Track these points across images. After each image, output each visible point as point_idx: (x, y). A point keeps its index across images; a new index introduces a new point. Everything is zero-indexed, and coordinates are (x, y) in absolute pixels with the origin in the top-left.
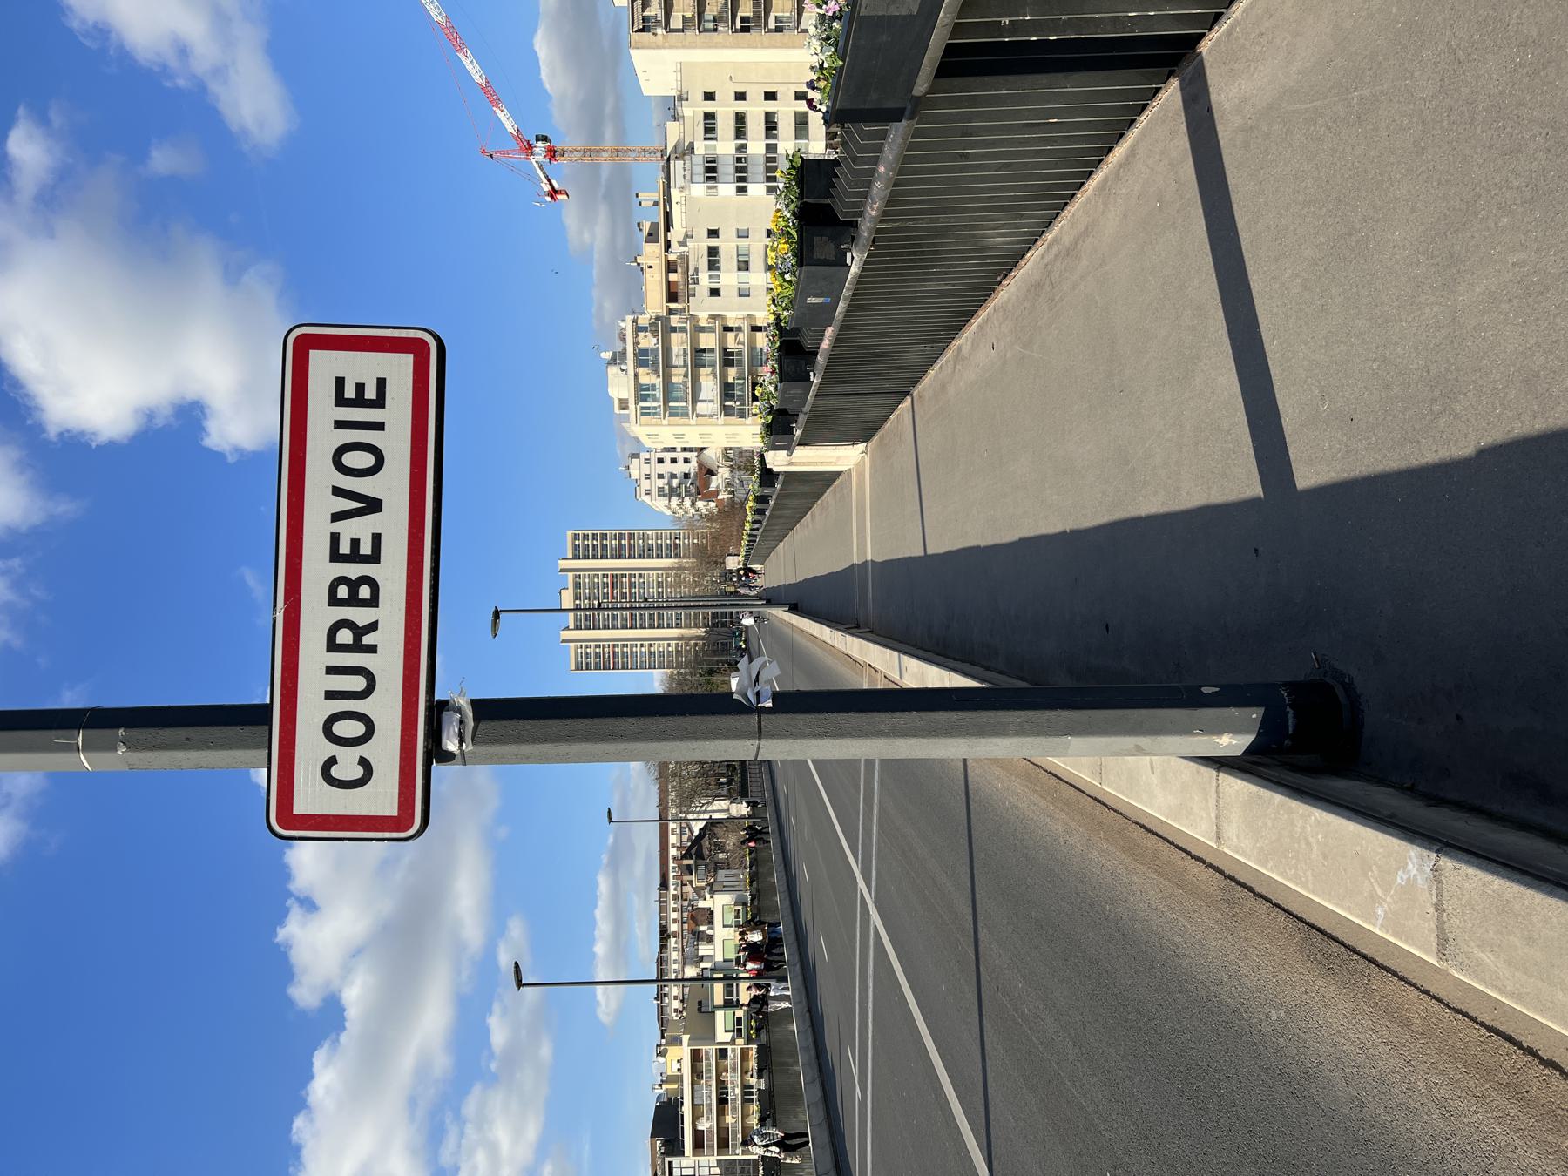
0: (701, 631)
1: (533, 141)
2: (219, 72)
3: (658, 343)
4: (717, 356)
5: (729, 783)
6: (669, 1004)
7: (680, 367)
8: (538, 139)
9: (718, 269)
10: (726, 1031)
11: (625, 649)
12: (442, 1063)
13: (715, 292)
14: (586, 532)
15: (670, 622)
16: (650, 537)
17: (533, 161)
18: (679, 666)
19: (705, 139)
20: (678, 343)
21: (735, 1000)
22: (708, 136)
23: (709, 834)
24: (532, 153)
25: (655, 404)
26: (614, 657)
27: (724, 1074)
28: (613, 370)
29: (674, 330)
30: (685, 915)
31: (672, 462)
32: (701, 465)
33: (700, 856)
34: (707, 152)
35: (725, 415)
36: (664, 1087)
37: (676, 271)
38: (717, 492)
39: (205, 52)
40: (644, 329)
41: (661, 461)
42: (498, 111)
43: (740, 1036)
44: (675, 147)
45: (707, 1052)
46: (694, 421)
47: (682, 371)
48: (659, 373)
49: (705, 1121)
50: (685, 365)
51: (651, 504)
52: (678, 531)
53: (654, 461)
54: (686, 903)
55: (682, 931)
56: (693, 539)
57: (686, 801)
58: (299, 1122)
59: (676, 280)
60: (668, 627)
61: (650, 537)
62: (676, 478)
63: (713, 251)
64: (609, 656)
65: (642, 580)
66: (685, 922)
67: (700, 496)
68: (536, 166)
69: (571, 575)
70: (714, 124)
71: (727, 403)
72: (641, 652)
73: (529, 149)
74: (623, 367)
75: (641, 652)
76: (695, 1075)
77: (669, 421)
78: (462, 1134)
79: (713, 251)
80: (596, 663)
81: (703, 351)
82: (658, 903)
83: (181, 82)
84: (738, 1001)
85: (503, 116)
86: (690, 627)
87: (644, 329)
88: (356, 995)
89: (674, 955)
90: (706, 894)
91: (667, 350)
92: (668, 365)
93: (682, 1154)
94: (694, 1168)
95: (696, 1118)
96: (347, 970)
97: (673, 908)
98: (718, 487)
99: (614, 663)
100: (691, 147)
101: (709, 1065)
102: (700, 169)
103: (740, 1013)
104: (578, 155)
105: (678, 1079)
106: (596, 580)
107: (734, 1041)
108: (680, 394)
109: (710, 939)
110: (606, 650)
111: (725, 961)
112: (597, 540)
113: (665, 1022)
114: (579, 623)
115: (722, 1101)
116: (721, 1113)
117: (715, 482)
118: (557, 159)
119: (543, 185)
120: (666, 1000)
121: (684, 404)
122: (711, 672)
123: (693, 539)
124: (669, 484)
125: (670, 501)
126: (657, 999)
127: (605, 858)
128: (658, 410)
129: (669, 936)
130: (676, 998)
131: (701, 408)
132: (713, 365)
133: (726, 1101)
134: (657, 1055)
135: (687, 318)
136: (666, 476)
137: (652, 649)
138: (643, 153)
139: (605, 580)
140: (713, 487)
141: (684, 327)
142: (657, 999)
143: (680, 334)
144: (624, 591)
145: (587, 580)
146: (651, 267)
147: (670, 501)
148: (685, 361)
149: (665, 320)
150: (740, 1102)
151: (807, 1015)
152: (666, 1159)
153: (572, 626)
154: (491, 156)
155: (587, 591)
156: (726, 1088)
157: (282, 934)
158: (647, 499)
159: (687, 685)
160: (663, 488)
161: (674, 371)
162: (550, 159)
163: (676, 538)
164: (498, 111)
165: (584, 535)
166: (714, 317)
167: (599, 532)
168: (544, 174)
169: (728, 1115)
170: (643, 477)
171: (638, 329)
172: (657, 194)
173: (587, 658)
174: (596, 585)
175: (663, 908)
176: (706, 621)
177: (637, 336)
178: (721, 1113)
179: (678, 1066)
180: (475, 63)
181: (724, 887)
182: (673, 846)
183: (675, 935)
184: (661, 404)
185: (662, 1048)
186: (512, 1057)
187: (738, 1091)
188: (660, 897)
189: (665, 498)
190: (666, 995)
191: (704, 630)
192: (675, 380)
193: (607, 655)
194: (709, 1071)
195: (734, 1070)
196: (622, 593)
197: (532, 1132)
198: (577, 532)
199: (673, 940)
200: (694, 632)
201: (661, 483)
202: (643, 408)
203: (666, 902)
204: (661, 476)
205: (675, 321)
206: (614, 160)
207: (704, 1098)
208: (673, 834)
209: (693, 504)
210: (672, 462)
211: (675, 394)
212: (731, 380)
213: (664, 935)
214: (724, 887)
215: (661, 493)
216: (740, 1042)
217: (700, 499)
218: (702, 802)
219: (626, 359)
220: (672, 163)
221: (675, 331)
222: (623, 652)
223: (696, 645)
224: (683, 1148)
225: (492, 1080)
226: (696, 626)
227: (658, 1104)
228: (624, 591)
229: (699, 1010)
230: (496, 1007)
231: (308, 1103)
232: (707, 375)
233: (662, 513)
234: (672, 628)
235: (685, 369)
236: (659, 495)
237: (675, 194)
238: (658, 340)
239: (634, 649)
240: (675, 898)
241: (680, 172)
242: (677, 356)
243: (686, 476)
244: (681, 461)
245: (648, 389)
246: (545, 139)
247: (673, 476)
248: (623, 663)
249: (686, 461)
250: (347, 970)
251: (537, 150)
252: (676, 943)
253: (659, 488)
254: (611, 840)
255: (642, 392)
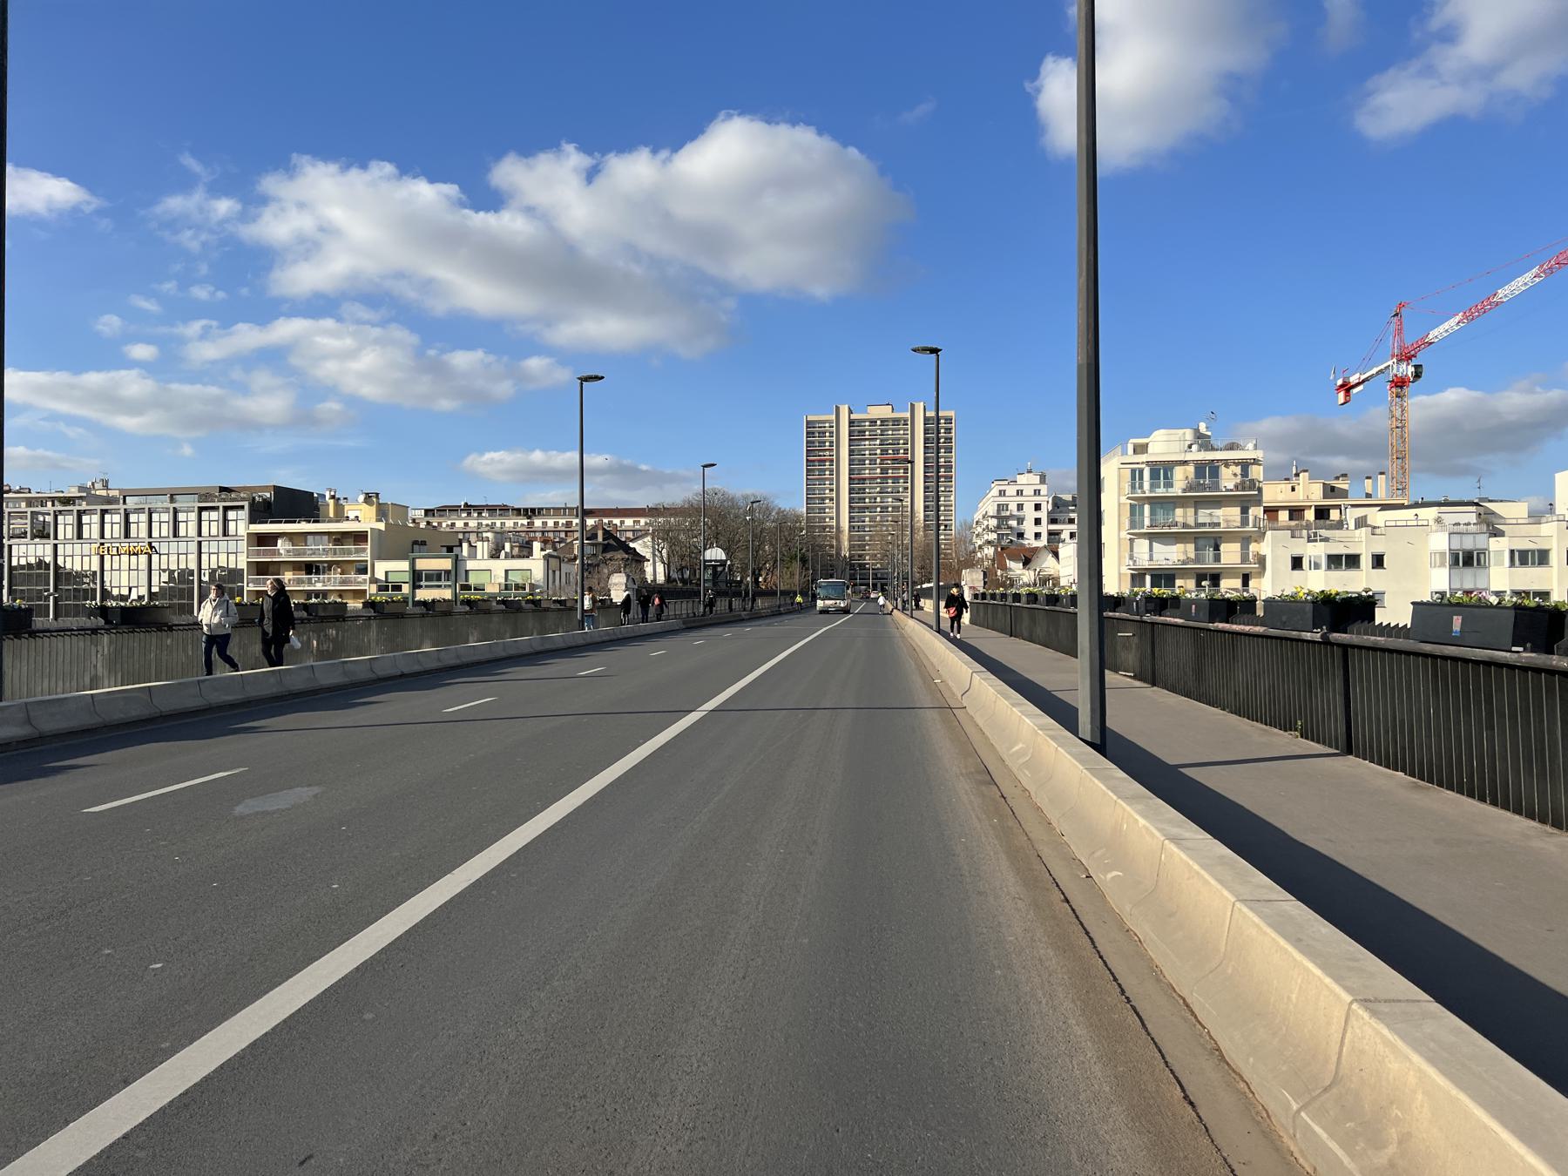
0: (845, 552)
1: (1415, 361)
2: (1429, 71)
3: (1227, 490)
4: (1210, 565)
5: (683, 581)
6: (460, 518)
7: (1196, 519)
8: (1416, 367)
9: (1329, 568)
10: (387, 573)
11: (827, 473)
12: (439, 307)
13: (1297, 563)
14: (953, 431)
15: (856, 520)
16: (947, 499)
17: (1390, 363)
18: (810, 528)
19: (1512, 552)
20: (1228, 516)
21: (422, 583)
22: (1517, 554)
23: (628, 559)
24: (1399, 361)
25: (1146, 486)
26: (819, 461)
27: (339, 570)
28: (1189, 435)
29: (1245, 511)
30: (551, 535)
31: (1036, 519)
32: (1035, 550)
33: (606, 548)
34: (1492, 554)
35: (1132, 575)
36: (331, 502)
37: (1291, 519)
38: (1004, 568)
39: (1451, 59)
40: (1245, 473)
41: (1038, 507)
42: (1457, 319)
43: (380, 589)
44: (1493, 513)
45: (364, 550)
46: (1124, 535)
47: (1191, 521)
48: (1189, 492)
49: (287, 547)
50: (1198, 525)
51: (989, 496)
52: (953, 528)
53: (1038, 499)
54: (563, 535)
55: (535, 532)
56: (945, 545)
57: (662, 534)
58: (389, 168)
59: (1280, 519)
60: (850, 518)
61: (947, 499)
62: (1018, 524)
63: (1353, 561)
64: (820, 456)
65: (901, 490)
66: (543, 534)
67: (999, 549)
68: (1382, 367)
69: (908, 415)
70: (1533, 563)
71: (1148, 578)
72: (825, 489)
73: (1406, 357)
74: (1195, 447)
75: (825, 489)
76: (339, 537)
77: (1124, 504)
78: (373, 325)
79: (1353, 561)
80: (813, 442)
81: (1217, 548)
82: (564, 506)
83: (1417, 35)
84: (420, 587)
85: (1451, 324)
86: (850, 541)
87: (1245, 473)
88: (509, 224)
89: (509, 524)
90: (548, 551)
91: (1218, 502)
92: (1199, 503)
93: (253, 520)
94: (236, 535)
95: (291, 537)
96: (530, 211)
97: (558, 522)
98: (1010, 569)
99: (814, 461)
100: (1497, 533)
101: (349, 553)
102: (1468, 543)
103: (406, 589)
104: (1398, 414)
105: (340, 516)
106: (901, 442)
107: (376, 583)
108: (1160, 518)
109: (495, 555)
110: (828, 453)
111: (467, 572)
112: (944, 443)
113: (442, 513)
114: (856, 520)
115: (310, 568)
116: (295, 566)
117: (1016, 567)
118: (1393, 390)
119: (1357, 375)
120: (464, 515)
121: (1147, 522)
122: (804, 561)
123: (945, 545)
124: (1011, 517)
125: (992, 517)
126: (466, 505)
127: (627, 462)
128: (1139, 491)
129: (529, 518)
130: (466, 524)
131: (1142, 546)
132: (1197, 560)
133: (309, 572)
134: (367, 494)
135: (1259, 528)
136: (1020, 513)
137: (827, 501)
138: (1400, 487)
139: (902, 451)
140: (1011, 564)
141: (1248, 524)
142: (466, 505)
143: (1238, 518)
144: (890, 471)
145: (902, 432)
146: (1293, 489)
147: (992, 517)
148: (1204, 525)
149: (1258, 500)
150: (306, 588)
151: (399, 673)
152: (247, 503)
153: (853, 417)
154: (1397, 315)
155: (890, 432)
156: (324, 573)
157: (570, 148)
158: (995, 492)
159: (789, 535)
160: (1007, 510)
161: (1191, 511)
162: (1393, 381)
163: (946, 526)
164: (1457, 319)
165: (951, 429)
166: (1261, 560)
167: (953, 444)
168: (1372, 376)
169: (294, 575)
170: (1019, 488)
171: (1245, 465)
172: (1384, 496)
173: (819, 433)
174: (896, 442)
175: (558, 511)
176: (857, 558)
177: (1237, 464)
178: (295, 566)
179: (352, 517)
180: (1523, 288)
181: (554, 572)
182: (622, 522)
183: (531, 524)
184: (1147, 495)
185: (375, 500)
186: (439, 370)
187: (319, 586)
188: (569, 509)
189: (996, 512)
190: (469, 514)
191: (847, 555)
192: (1179, 512)
193: (822, 454)
194: (343, 552)
195: (343, 582)
196: (888, 469)
197: (368, 391)
198: (953, 421)
199: (525, 522)
200: (846, 544)
201: (1013, 507)
202: (1141, 471)
203: (565, 514)
204: (1020, 507)
205: (1256, 512)
206: (1392, 455)
207: (313, 547)
208: (634, 522)
209: (989, 542)
210: (1036, 519)
211: (1160, 512)
212: (1178, 582)
213: (531, 513)
214: (554, 572)
215: (1001, 507)
216: (373, 589)
217: (996, 550)
218: (664, 551)
219: (1205, 450)
220: (1473, 509)
221: (1242, 513)
222: (825, 470)
223: (832, 546)
224: (259, 523)
225: (419, 353)
226: (851, 547)
227: (315, 495)
228: (890, 471)
229: (415, 543)
230: (491, 358)
231: (404, 178)
232: (1185, 552)
233: (976, 510)
234: (850, 522)
235: (1193, 524)
236: (998, 505)
237: (1429, 513)
238: (1231, 490)
239: (827, 482)
240: (569, 524)
241: (1463, 518)
242: (1210, 514)
243: (1021, 535)
244: (1038, 529)
245: (1166, 477)
246: (1417, 375)
247: (1020, 520)
248: (813, 470)
249: (1038, 535)
250: (530, 211)
251: (1404, 366)
252: (522, 525)
253: (1007, 505)
254: (644, 467)
255: (1162, 471)
